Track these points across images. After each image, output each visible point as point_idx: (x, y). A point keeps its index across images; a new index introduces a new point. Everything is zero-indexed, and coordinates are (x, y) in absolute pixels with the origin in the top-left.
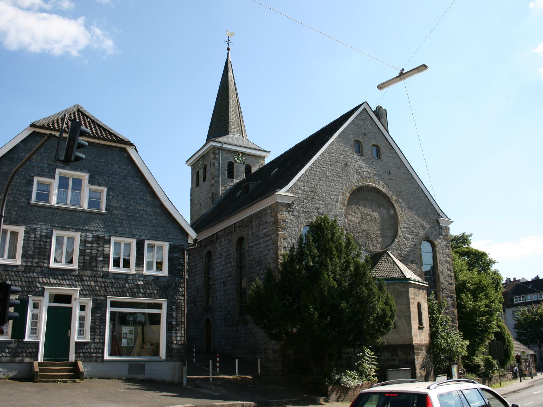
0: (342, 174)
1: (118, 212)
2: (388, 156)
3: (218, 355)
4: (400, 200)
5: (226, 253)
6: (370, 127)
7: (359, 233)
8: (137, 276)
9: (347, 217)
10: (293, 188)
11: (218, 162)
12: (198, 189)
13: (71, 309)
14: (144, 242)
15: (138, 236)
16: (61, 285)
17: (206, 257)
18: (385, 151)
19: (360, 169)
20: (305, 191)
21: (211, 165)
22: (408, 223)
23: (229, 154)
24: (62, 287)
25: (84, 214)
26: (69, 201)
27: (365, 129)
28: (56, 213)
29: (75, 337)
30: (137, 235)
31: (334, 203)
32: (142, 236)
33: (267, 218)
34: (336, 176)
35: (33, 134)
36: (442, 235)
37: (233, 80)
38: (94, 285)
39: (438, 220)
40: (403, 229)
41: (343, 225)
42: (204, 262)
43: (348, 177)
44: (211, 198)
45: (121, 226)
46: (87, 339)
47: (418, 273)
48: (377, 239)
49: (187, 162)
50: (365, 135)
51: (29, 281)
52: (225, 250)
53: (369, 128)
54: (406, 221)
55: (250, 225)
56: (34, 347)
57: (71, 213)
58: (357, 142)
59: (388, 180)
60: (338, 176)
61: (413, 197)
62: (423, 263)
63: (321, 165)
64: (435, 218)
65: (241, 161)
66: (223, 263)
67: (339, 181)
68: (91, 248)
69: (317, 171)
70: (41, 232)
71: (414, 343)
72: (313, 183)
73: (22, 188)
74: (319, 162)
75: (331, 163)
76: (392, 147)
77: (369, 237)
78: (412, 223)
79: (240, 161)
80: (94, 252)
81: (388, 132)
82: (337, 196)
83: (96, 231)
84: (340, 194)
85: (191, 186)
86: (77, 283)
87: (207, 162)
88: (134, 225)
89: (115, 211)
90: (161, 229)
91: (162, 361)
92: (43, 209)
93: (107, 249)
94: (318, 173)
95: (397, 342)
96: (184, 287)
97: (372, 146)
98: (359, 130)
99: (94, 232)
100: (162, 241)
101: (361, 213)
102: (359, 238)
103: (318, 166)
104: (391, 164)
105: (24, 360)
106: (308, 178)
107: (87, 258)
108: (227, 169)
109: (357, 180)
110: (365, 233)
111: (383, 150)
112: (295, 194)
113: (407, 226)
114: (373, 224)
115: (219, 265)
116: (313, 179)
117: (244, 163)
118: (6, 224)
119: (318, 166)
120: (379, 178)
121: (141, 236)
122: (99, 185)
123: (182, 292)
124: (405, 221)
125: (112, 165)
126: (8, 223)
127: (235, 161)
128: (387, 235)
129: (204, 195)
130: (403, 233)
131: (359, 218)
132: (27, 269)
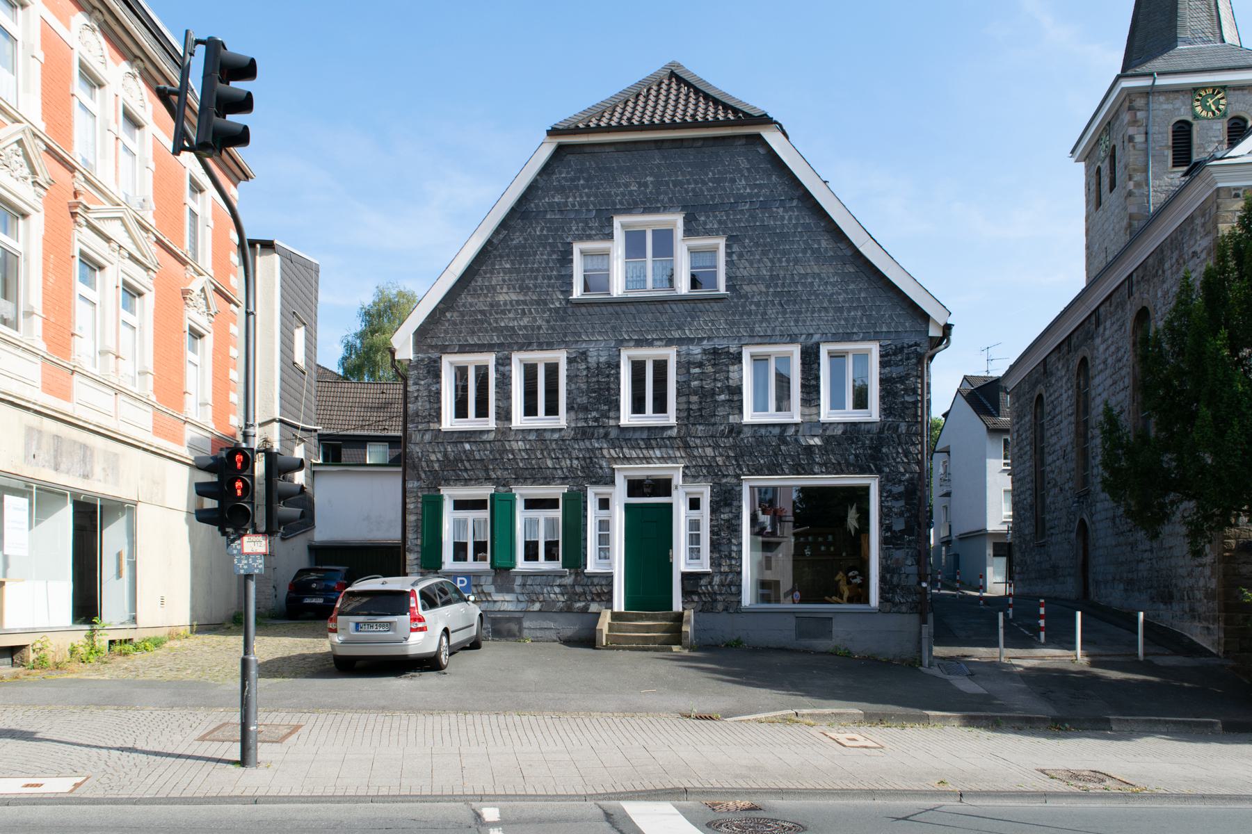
1: (755, 288)
8: (807, 426)
12: (1101, 212)
13: (669, 507)
14: (819, 348)
15: (804, 336)
16: (648, 460)
17: (1078, 375)
24: (648, 463)
25: (680, 306)
26: (650, 284)
28: (624, 312)
29: (682, 562)
30: (801, 334)
32: (812, 334)
33: (1196, 241)
35: (560, 150)
38: (712, 454)
42: (1075, 386)
44: (1126, 229)
45: (764, 320)
46: (704, 565)
49: (1072, 152)
51: (584, 458)
52: (1112, 349)
55: (1160, 272)
56: (603, 583)
57: (653, 307)
65: (1213, 113)
66: (1110, 381)
68: (700, 378)
70: (599, 355)
73: (552, 271)
79: (1210, 114)
80: (707, 384)
83: (709, 338)
85: (1087, 211)
86: (678, 454)
88: (792, 312)
89: (747, 288)
90: (859, 313)
91: (872, 613)
92: (597, 309)
93: (733, 375)
96: (922, 443)
99: (705, 342)
100: (863, 340)
105: (588, 609)
107: (694, 399)
108: (1170, 143)
115: (1100, 389)
117: (1224, 115)
118: (532, 350)
121: (810, 335)
122: (708, 233)
123: (917, 454)
125: (733, 181)
126: (535, 348)
127: (1196, 117)
132: (583, 434)
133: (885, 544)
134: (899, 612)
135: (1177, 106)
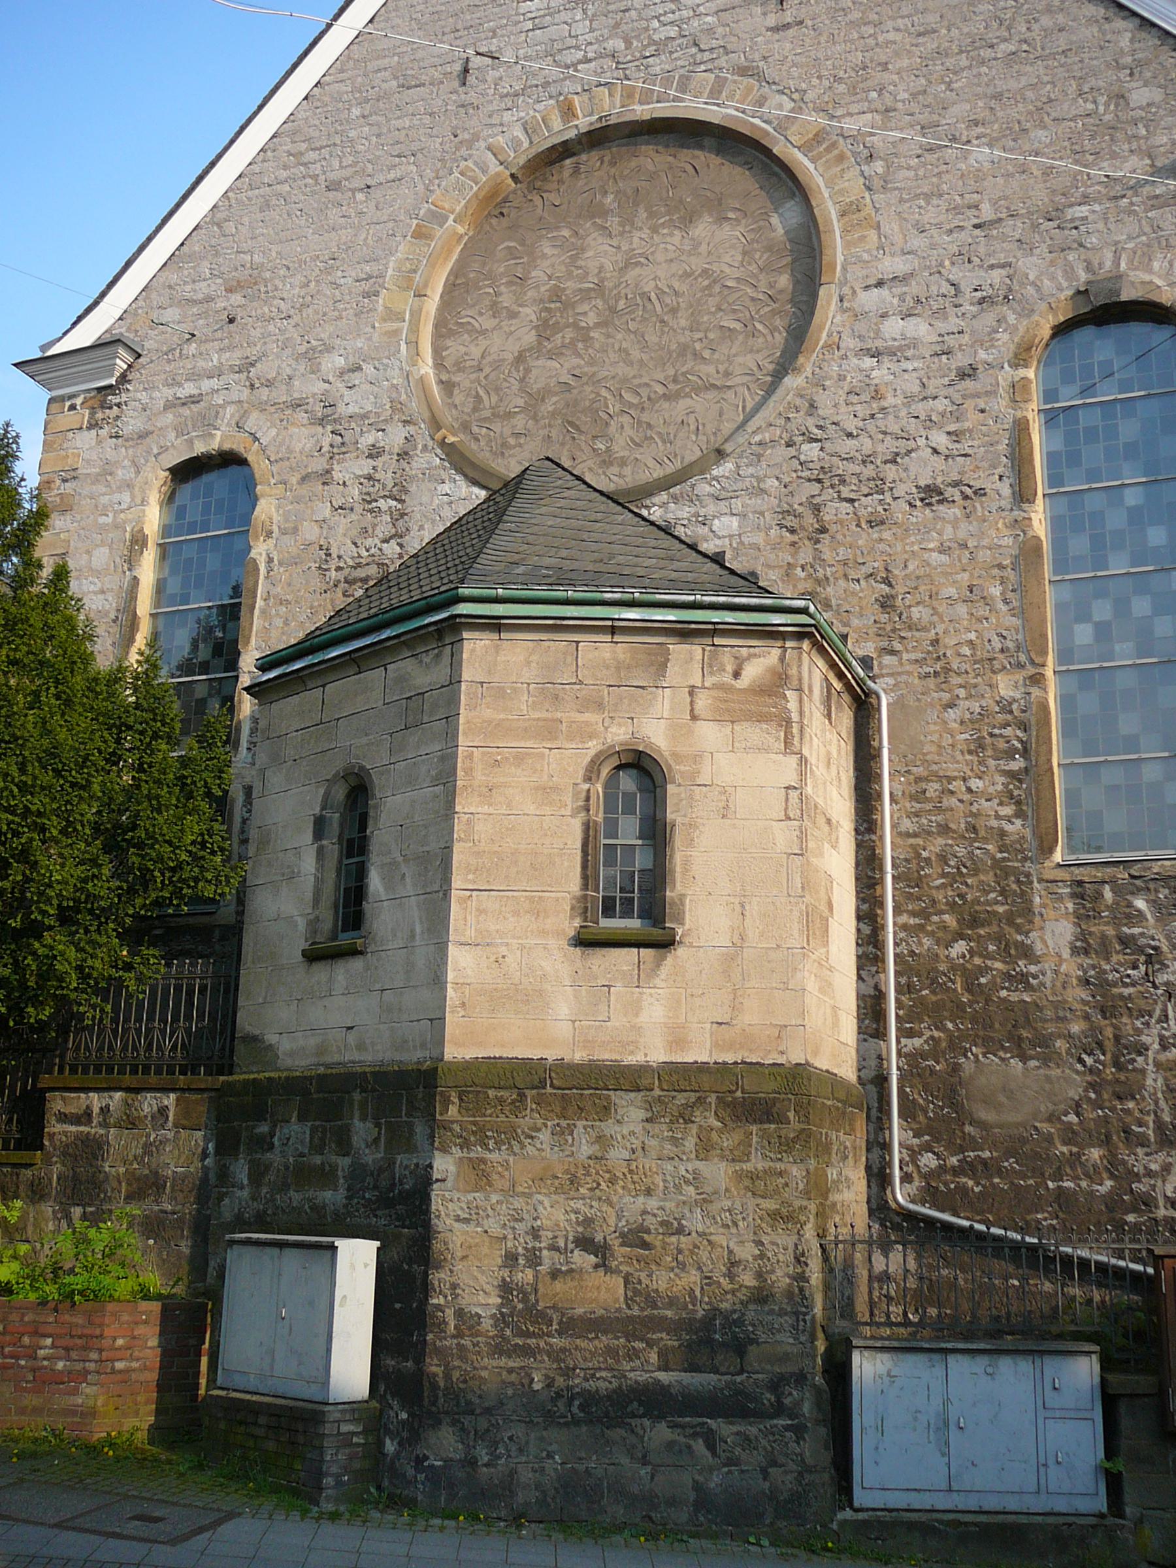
60: (399, 156)
71: (451, 1053)
95: (361, 1047)
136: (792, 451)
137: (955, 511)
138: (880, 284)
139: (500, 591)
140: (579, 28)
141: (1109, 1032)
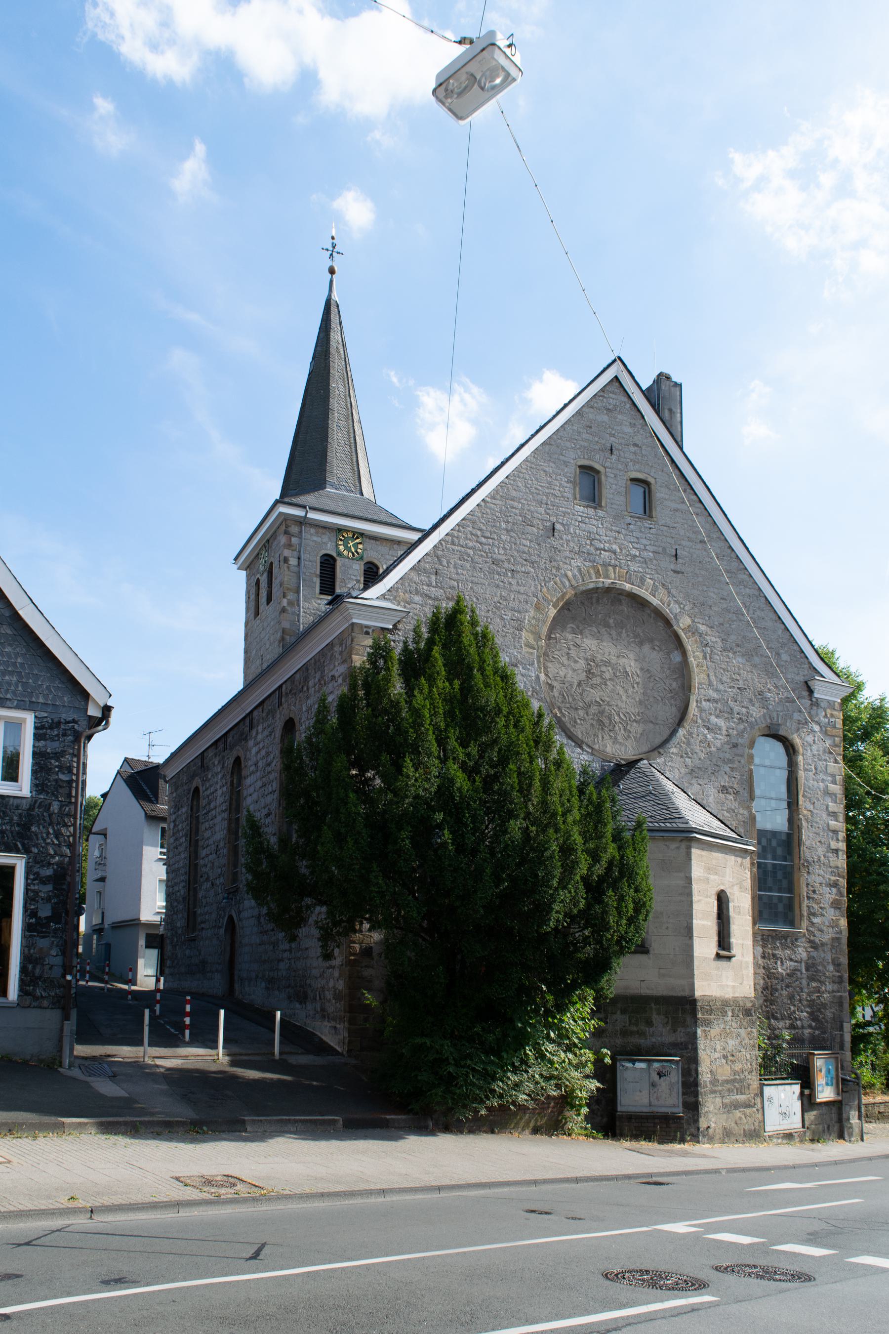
0: (539, 556)
2: (676, 510)
3: (188, 998)
4: (702, 628)
5: (265, 761)
6: (628, 430)
7: (576, 709)
9: (546, 668)
10: (398, 588)
11: (296, 554)
18: (667, 497)
19: (591, 545)
20: (430, 598)
21: (282, 563)
22: (721, 687)
23: (324, 536)
27: (613, 436)
31: (512, 630)
34: (519, 559)
36: (818, 723)
37: (342, 352)
39: (809, 683)
40: (703, 702)
41: (533, 687)
42: (229, 784)
43: (553, 564)
44: (280, 642)
47: (740, 817)
48: (628, 727)
49: (236, 559)
50: (612, 453)
52: (263, 753)
53: (624, 433)
54: (715, 683)
55: (305, 688)
58: (588, 471)
59: (671, 573)
60: (526, 560)
61: (740, 621)
62: (757, 792)
63: (481, 530)
64: (802, 679)
66: (259, 784)
67: (528, 573)
69: (467, 547)
71: (698, 994)
72: (455, 576)
74: (474, 522)
75: (510, 526)
76: (689, 484)
77: (606, 721)
78: (730, 687)
79: (350, 554)
81: (681, 448)
82: (519, 612)
84: (528, 607)
85: (246, 617)
87: (273, 557)
94: (471, 552)
96: (74, 825)
97: (629, 482)
98: (596, 439)
101: (586, 659)
102: (575, 722)
103: (472, 534)
104: (682, 532)
106: (441, 564)
108: (318, 572)
109: (580, 570)
110: (594, 709)
111: (659, 493)
112: (402, 604)
113: (715, 695)
114: (618, 687)
115: (251, 790)
116: (455, 567)
117: (361, 558)
119: (472, 534)
120: (643, 568)
124: (710, 684)
127: (339, 554)
128: (656, 718)
129: (267, 638)
130: (704, 715)
131: (580, 671)
133: (29, 931)
134: (40, 1007)
135: (324, 540)
136: (682, 760)
137: (731, 797)
138: (709, 700)
139: (668, 825)
140: (602, 532)
141: (770, 984)
